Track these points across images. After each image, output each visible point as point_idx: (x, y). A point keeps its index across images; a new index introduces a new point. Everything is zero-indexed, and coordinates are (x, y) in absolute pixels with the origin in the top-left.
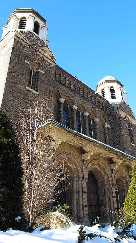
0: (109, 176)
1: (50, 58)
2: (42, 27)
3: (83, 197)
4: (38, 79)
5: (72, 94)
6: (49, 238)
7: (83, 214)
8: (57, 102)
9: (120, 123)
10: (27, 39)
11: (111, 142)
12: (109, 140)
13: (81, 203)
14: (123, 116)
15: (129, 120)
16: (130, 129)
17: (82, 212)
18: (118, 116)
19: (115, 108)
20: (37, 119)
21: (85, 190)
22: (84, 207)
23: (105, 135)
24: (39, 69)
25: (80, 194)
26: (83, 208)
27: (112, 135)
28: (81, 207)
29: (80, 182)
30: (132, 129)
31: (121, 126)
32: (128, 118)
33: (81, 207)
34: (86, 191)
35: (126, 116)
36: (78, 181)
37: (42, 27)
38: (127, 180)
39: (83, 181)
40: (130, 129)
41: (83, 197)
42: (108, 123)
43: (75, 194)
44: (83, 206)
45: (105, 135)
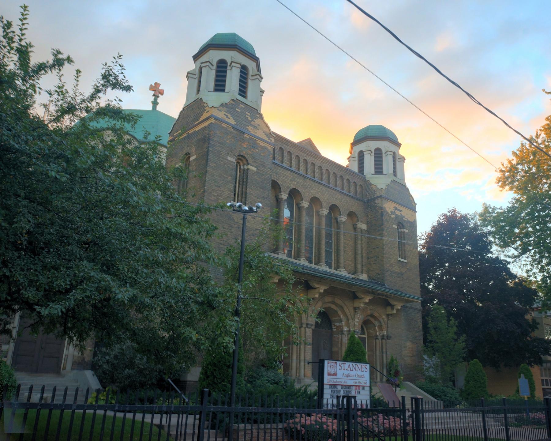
0: (350, 317)
1: (266, 139)
2: (252, 76)
3: (305, 350)
4: (247, 182)
5: (301, 181)
6: (401, 401)
7: (304, 374)
8: (275, 200)
9: (382, 224)
10: (229, 116)
11: (364, 255)
12: (362, 252)
13: (302, 358)
14: (389, 211)
15: (401, 214)
16: (402, 230)
17: (302, 371)
18: (380, 211)
19: (377, 195)
20: (243, 182)
21: (310, 340)
22: (306, 364)
23: (356, 243)
24: (248, 164)
25: (302, 347)
26: (305, 365)
27: (368, 243)
28: (302, 364)
29: (303, 329)
30: (405, 230)
31: (383, 230)
32: (401, 211)
33: (302, 364)
34: (311, 342)
35: (396, 209)
36: (300, 328)
37: (252, 76)
38: (382, 321)
39: (307, 327)
40: (402, 230)
41: (305, 350)
42: (362, 222)
43: (295, 346)
44: (305, 363)
45: (356, 243)
